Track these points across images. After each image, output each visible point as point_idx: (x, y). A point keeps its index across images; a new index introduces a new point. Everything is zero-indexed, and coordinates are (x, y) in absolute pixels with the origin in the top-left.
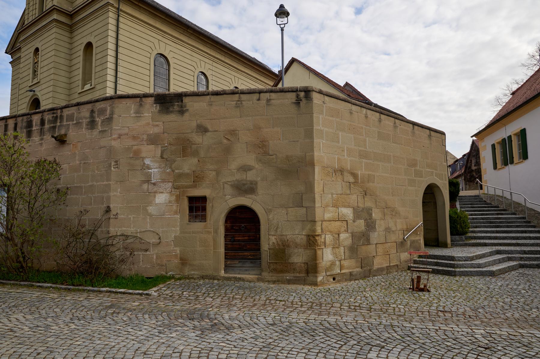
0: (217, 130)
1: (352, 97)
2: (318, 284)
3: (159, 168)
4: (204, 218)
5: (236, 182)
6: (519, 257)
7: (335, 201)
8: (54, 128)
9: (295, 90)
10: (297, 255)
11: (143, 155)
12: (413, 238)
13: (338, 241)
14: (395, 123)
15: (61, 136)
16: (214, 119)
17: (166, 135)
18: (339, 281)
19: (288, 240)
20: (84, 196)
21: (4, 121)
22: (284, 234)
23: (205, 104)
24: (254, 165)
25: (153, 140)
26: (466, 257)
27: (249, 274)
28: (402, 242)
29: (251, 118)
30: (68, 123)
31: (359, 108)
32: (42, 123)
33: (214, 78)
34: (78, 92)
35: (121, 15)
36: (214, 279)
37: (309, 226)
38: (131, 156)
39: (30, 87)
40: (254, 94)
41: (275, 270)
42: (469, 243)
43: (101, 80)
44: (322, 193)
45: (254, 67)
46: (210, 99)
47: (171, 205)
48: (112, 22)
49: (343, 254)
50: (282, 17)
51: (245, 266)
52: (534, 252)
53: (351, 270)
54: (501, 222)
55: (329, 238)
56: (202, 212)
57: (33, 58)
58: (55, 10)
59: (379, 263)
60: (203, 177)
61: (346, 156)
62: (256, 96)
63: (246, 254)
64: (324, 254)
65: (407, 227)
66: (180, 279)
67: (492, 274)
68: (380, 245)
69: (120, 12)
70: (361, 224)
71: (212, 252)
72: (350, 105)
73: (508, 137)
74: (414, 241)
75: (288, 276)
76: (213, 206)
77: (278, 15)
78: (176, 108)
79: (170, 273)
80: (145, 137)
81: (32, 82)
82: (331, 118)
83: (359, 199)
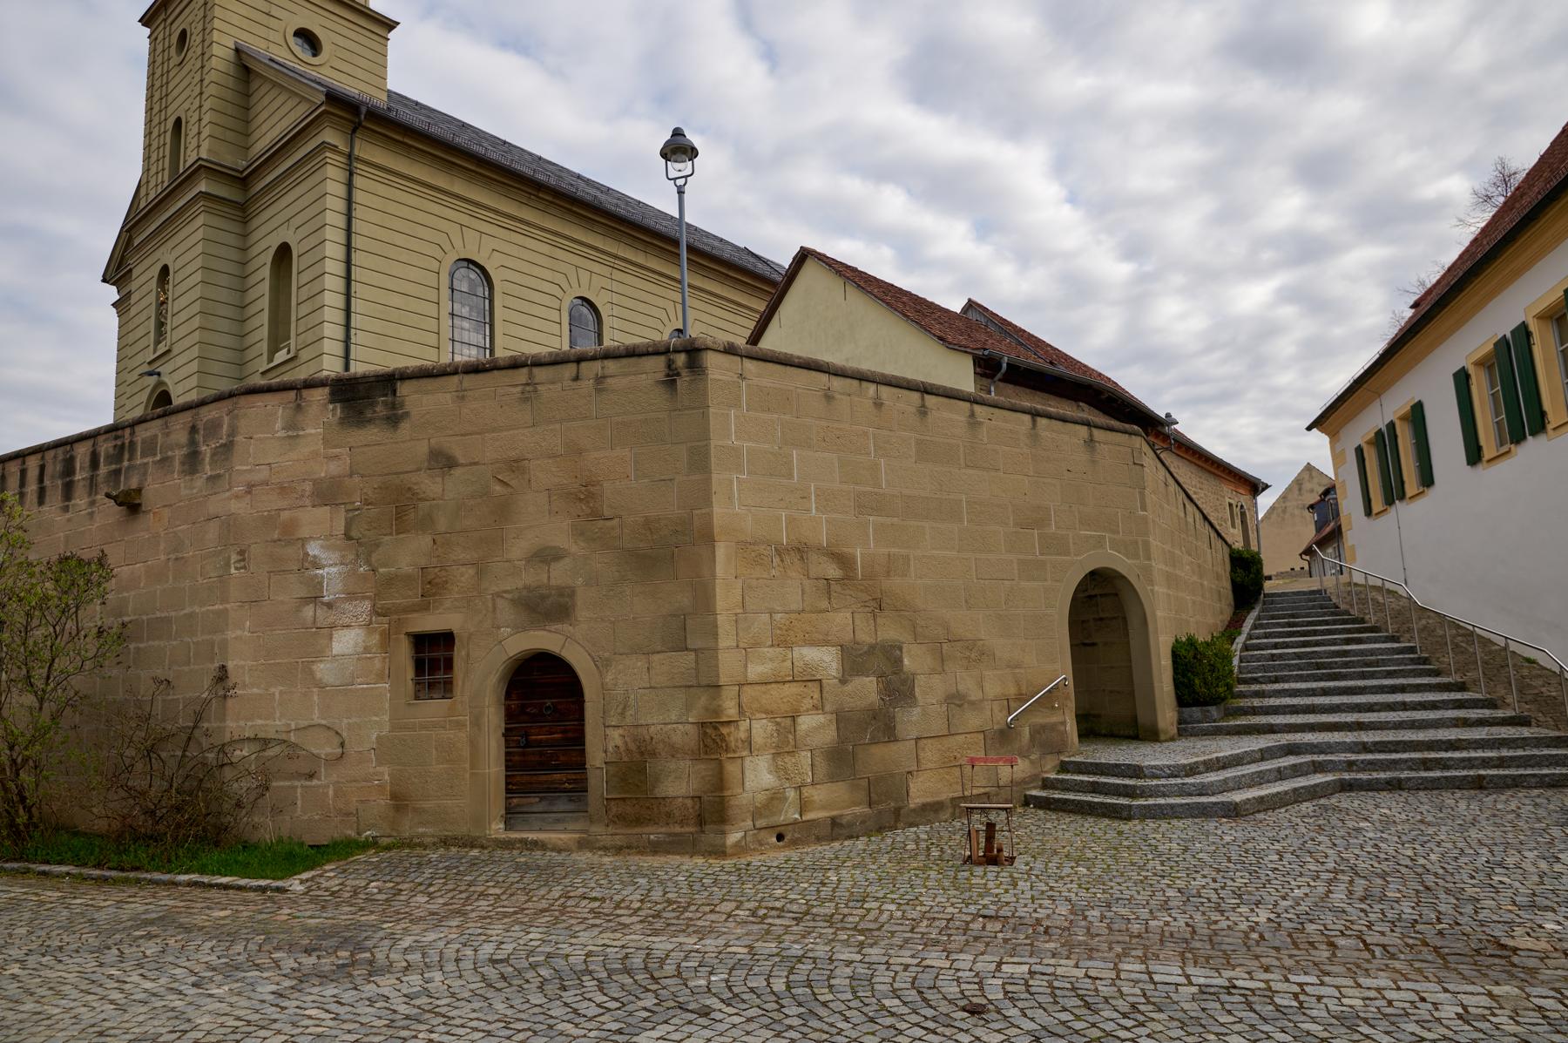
0: (477, 460)
1: (950, 343)
2: (729, 851)
3: (341, 564)
4: (447, 689)
5: (525, 593)
6: (1344, 762)
7: (780, 629)
8: (117, 473)
9: (662, 349)
10: (676, 778)
11: (304, 532)
12: (1040, 719)
13: (791, 737)
14: (972, 415)
15: (127, 493)
16: (471, 434)
17: (356, 479)
18: (795, 843)
19: (652, 738)
20: (174, 643)
21: (19, 461)
22: (642, 722)
23: (448, 396)
24: (567, 547)
25: (327, 494)
26: (1174, 767)
27: (565, 830)
28: (1001, 732)
29: (558, 426)
30: (145, 460)
31: (855, 382)
32: (94, 464)
33: (616, 312)
34: (261, 371)
35: (358, 171)
36: (473, 847)
37: (703, 699)
38: (276, 537)
39: (150, 363)
40: (564, 366)
41: (622, 820)
42: (1227, 726)
43: (310, 337)
44: (741, 611)
45: (728, 275)
46: (461, 383)
47: (369, 658)
48: (336, 188)
49: (809, 768)
50: (679, 159)
51: (555, 809)
52: (1389, 746)
53: (834, 813)
54: (1346, 665)
55: (761, 729)
56: (445, 674)
57: (157, 287)
58: (202, 170)
59: (921, 791)
60: (446, 582)
61: (814, 511)
62: (569, 370)
63: (557, 777)
64: (747, 773)
65: (1019, 689)
66: (388, 848)
67: (1233, 812)
68: (929, 741)
69: (355, 164)
70: (867, 689)
71: (468, 776)
72: (824, 377)
73: (1387, 426)
74: (1044, 727)
75: (654, 833)
76: (468, 655)
77: (669, 156)
78: (380, 410)
79: (368, 833)
80: (308, 487)
81: (155, 352)
82: (765, 416)
83: (857, 622)
